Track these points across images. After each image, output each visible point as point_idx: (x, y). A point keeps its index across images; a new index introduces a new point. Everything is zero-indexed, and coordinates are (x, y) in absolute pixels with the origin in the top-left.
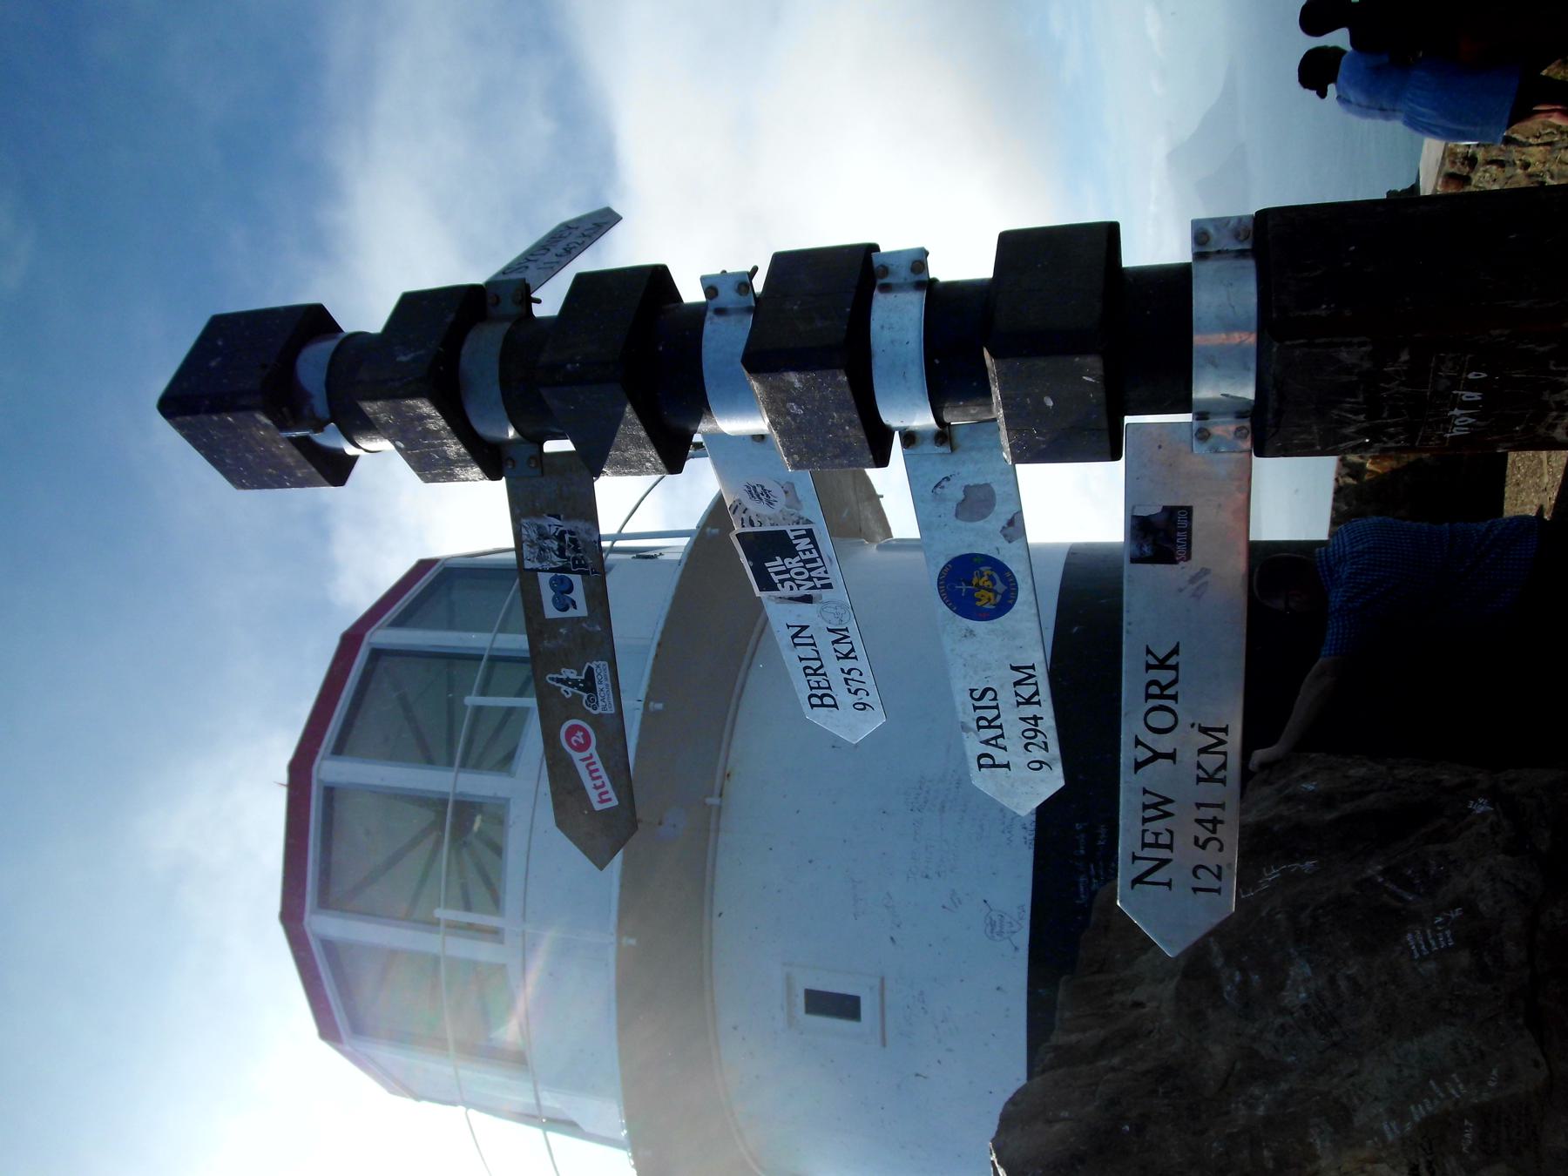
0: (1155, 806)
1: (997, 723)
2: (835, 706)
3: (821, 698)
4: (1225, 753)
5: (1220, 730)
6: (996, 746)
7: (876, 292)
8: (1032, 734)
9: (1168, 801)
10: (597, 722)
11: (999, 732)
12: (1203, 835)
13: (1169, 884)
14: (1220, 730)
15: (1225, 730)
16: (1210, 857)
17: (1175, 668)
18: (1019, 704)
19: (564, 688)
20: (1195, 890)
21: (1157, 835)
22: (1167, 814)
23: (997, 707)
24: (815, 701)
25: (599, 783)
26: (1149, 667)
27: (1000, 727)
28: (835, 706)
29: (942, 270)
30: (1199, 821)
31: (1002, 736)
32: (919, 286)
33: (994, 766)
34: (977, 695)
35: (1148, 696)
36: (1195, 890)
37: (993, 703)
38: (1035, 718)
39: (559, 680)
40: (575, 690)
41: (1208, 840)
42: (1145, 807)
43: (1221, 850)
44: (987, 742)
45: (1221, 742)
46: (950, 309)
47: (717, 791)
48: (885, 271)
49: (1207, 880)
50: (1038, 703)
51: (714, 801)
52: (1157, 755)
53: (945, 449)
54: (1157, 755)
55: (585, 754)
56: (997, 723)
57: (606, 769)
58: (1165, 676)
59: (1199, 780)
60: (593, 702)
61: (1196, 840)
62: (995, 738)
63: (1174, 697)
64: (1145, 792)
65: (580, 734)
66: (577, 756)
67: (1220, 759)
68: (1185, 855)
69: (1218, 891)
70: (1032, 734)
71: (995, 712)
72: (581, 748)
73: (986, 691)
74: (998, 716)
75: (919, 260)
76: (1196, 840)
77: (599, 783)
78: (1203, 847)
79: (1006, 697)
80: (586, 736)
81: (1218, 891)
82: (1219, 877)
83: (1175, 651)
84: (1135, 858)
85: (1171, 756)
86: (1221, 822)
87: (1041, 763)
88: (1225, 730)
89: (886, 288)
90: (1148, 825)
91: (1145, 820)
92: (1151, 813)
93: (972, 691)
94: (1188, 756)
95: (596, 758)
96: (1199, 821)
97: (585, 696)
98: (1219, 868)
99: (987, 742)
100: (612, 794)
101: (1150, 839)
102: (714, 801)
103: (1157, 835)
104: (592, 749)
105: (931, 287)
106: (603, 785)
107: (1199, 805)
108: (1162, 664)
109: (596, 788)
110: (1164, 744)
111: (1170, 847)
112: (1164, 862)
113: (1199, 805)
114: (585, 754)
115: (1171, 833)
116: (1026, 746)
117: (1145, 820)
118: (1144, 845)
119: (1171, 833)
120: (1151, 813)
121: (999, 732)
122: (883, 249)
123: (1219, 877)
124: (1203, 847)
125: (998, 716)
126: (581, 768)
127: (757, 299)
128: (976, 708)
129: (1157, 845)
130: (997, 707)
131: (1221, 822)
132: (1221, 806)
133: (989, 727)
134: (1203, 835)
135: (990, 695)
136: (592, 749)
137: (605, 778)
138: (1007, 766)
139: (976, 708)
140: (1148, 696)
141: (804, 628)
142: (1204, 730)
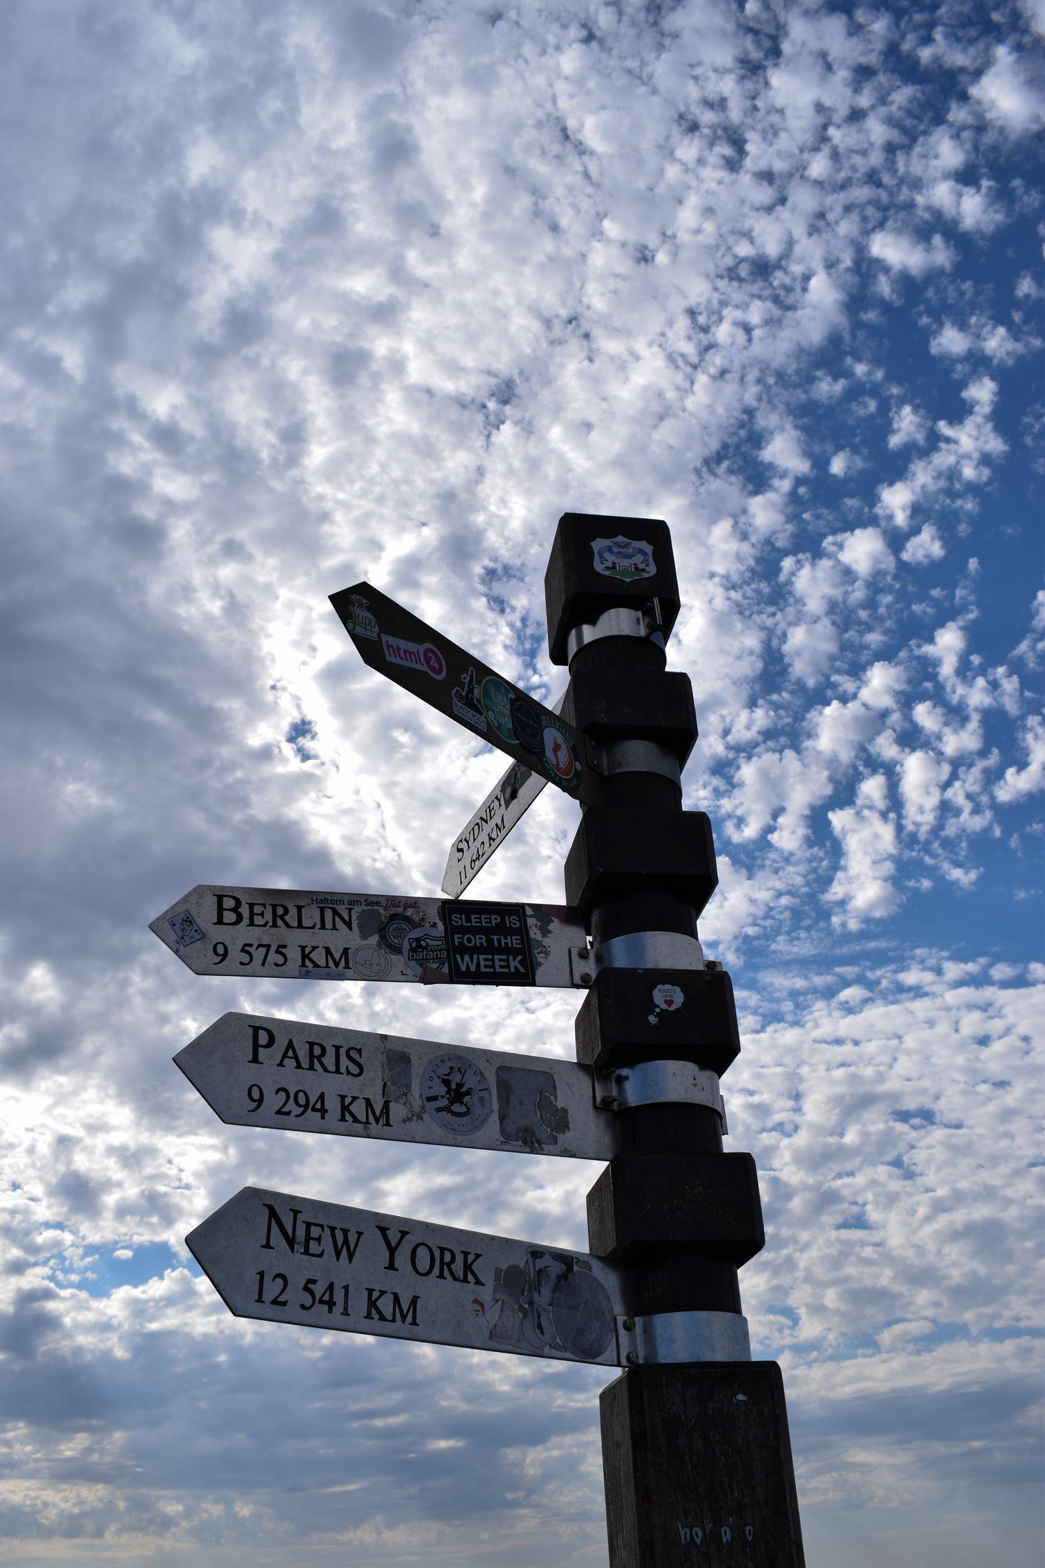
0: (346, 1242)
3: (235, 910)
4: (394, 1321)
5: (414, 1318)
6: (285, 1056)
8: (302, 1100)
9: (351, 1256)
12: (319, 1289)
14: (414, 1318)
15: (414, 1323)
17: (465, 1280)
20: (261, 1274)
22: (338, 1253)
26: (466, 1254)
27: (311, 1068)
30: (331, 1287)
31: (299, 1066)
33: (256, 1046)
34: (354, 1054)
36: (261, 1274)
41: (313, 1295)
42: (345, 1232)
43: (303, 1307)
44: (290, 1045)
45: (404, 1318)
52: (392, 1251)
54: (392, 1251)
58: (458, 1267)
61: (314, 1282)
63: (441, 1276)
64: (360, 1234)
69: (260, 1300)
74: (326, 1070)
76: (314, 1282)
78: (306, 1288)
79: (348, 1086)
81: (260, 1300)
82: (275, 1302)
83: (478, 1282)
85: (391, 1266)
86: (330, 1311)
87: (260, 1101)
90: (327, 1231)
91: (333, 1229)
92: (340, 1238)
93: (359, 1051)
96: (331, 1287)
99: (290, 1045)
101: (315, 1232)
103: (319, 1240)
107: (346, 1288)
108: (468, 1268)
110: (402, 1257)
112: (291, 1242)
113: (346, 1288)
115: (320, 1256)
118: (309, 1225)
119: (320, 1256)
121: (306, 1065)
123: (275, 1302)
124: (306, 1288)
128: (337, 1048)
129: (308, 1238)
131: (330, 1311)
134: (319, 1289)
135: (354, 1069)
138: (255, 1060)
139: (337, 1048)
140: (442, 1250)
142: (414, 1302)
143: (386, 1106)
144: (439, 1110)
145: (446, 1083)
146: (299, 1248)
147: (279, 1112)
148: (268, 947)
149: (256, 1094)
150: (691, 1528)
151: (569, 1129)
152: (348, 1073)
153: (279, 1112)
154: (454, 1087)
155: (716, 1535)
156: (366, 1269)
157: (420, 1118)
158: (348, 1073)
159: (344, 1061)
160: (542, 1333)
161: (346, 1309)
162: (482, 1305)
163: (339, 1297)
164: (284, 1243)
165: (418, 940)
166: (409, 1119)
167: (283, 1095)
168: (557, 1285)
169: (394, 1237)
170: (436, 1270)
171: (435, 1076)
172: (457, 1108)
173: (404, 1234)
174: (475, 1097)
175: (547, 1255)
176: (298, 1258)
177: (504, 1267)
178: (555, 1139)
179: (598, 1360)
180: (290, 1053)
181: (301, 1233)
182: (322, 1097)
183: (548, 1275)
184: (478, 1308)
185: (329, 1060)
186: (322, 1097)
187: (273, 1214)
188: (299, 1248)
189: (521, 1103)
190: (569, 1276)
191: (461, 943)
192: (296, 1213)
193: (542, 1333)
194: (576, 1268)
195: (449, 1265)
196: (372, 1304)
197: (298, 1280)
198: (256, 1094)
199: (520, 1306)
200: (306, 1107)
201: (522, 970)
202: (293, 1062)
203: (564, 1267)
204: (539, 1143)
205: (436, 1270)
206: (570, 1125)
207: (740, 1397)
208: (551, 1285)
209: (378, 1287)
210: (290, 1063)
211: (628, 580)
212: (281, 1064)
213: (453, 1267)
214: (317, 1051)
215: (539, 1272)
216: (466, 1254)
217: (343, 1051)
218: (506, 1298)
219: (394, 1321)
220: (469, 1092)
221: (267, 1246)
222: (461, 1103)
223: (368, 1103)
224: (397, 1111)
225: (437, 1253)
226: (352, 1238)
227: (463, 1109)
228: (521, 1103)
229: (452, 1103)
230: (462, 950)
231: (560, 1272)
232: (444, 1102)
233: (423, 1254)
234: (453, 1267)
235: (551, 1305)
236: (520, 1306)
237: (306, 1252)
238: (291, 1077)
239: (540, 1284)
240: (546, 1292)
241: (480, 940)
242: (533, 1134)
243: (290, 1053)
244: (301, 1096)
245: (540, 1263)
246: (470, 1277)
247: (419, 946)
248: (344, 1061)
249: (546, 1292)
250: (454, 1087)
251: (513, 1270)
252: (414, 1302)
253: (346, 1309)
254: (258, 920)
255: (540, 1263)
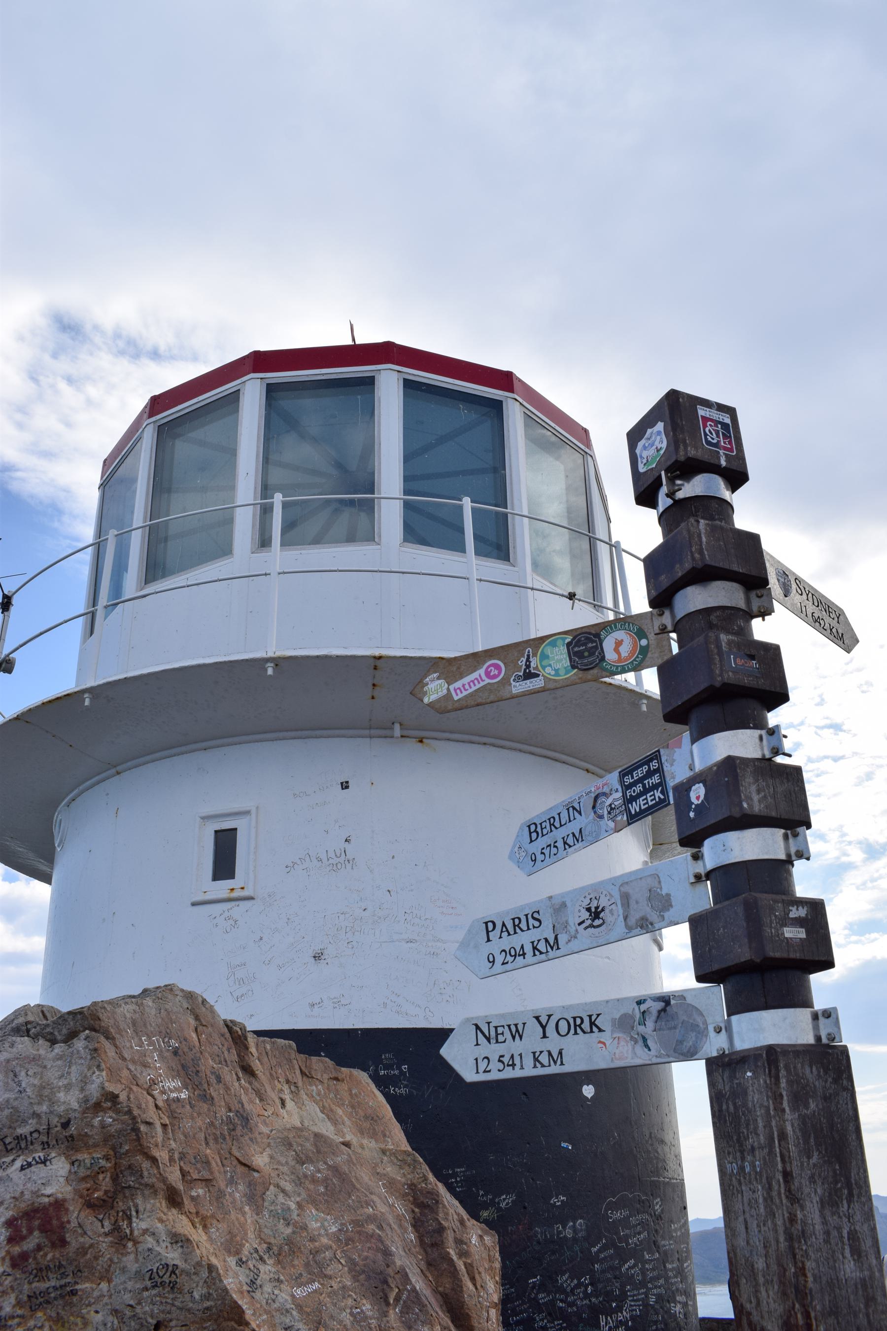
0: (517, 1031)
1: (518, 930)
2: (531, 841)
3: (536, 831)
4: (550, 1066)
5: (562, 1062)
6: (502, 931)
7: (783, 831)
8: (513, 953)
9: (521, 1037)
10: (505, 682)
11: (512, 932)
12: (506, 1060)
13: (477, 1044)
14: (562, 1062)
15: (562, 1064)
16: (495, 1065)
17: (592, 1031)
18: (533, 943)
19: (525, 660)
20: (476, 1059)
21: (502, 1034)
22: (514, 1038)
23: (529, 929)
24: (533, 828)
25: (467, 687)
26: (590, 1016)
27: (515, 933)
28: (531, 841)
29: (799, 868)
30: (512, 1057)
31: (509, 934)
32: (789, 855)
33: (488, 932)
34: (536, 915)
35: (575, 1018)
36: (476, 1059)
37: (531, 927)
38: (524, 954)
39: (528, 656)
40: (524, 667)
41: (503, 1063)
42: (516, 1025)
43: (499, 1071)
44: (504, 925)
45: (555, 1062)
46: (775, 873)
47: (405, 733)
48: (796, 835)
49: (482, 1065)
50: (535, 955)
51: (397, 731)
52: (544, 1027)
53: (693, 880)
54: (544, 1027)
55: (484, 677)
56: (518, 930)
57: (476, 691)
58: (586, 1026)
59: (534, 1053)
60: (518, 679)
61: (502, 1056)
62: (507, 931)
63: (576, 1033)
64: (524, 1024)
65: (496, 672)
66: (482, 671)
67: (546, 1063)
68: (493, 1050)
69: (477, 1072)
70: (513, 953)
71: (525, 928)
72: (487, 674)
73: (540, 921)
74: (522, 931)
75: (803, 854)
76: (502, 1056)
77: (467, 687)
78: (499, 1061)
79: (534, 935)
80: (495, 677)
81: (477, 1072)
82: (485, 1071)
83: (600, 1030)
84: (489, 1023)
85: (545, 1036)
86: (513, 1069)
87: (494, 961)
88: (562, 1064)
89: (786, 837)
90: (506, 1028)
91: (509, 1026)
92: (513, 1029)
93: (538, 912)
94: (546, 1045)
95: (482, 684)
96: (512, 1057)
97: (521, 674)
98: (489, 1071)
99: (504, 925)
100: (460, 696)
101: (500, 1030)
102: (397, 731)
103: (502, 1034)
104: (488, 681)
105: (789, 862)
106: (466, 690)
107: (521, 1055)
108: (592, 1024)
109: (464, 686)
111: (497, 1042)
112: (488, 1039)
113: (521, 1055)
114: (484, 677)
115: (504, 1042)
116: (504, 951)
117: (509, 1026)
118: (496, 1028)
119: (504, 1042)
120: (513, 1029)
121: (512, 932)
122: (808, 832)
123: (485, 1071)
124: (499, 1061)
125: (522, 931)
126: (475, 675)
127: (770, 759)
128: (526, 915)
129: (497, 1034)
130: (529, 929)
131: (513, 1069)
132: (522, 1068)
133: (514, 926)
135: (537, 924)
136: (488, 681)
137: (470, 691)
138: (489, 940)
139: (526, 915)
140: (575, 1018)
141: (580, 813)
142: (560, 1053)
143: (556, 938)
144: (586, 928)
145: (589, 910)
146: (493, 1041)
147: (503, 964)
148: (550, 845)
149: (491, 959)
150: (732, 1163)
151: (671, 906)
152: (534, 927)
153: (503, 964)
154: (593, 910)
155: (742, 1168)
156: (784, 1151)
157: (576, 937)
158: (534, 927)
159: (531, 921)
160: (650, 1050)
161: (522, 1066)
162: (604, 1044)
163: (517, 1060)
164: (485, 1040)
165: (610, 805)
166: (569, 941)
167: (503, 953)
168: (658, 1017)
169: (544, 1020)
170: (572, 1031)
171: (581, 908)
172: (597, 922)
173: (549, 1016)
174: (607, 911)
175: (649, 1000)
176: (494, 1046)
177: (617, 1017)
178: (663, 917)
179: (695, 1057)
180: (504, 929)
181: (493, 1033)
182: (522, 947)
183: (650, 1013)
184: (602, 1045)
185: (523, 925)
186: (522, 947)
187: (477, 1027)
188: (493, 1041)
189: (637, 902)
190: (668, 1008)
191: (631, 795)
192: (489, 1023)
193: (650, 1050)
194: (673, 1002)
195: (580, 1026)
196: (536, 1059)
197: (494, 1058)
198: (491, 959)
199: (632, 1037)
200: (515, 956)
201: (662, 797)
202: (506, 933)
203: (663, 1004)
204: (652, 924)
205: (572, 1031)
206: (673, 904)
207: (749, 1074)
208: (654, 1018)
209: (538, 1050)
210: (505, 934)
211: (654, 466)
212: (501, 937)
213: (583, 1026)
214: (517, 921)
215: (644, 1012)
216: (590, 1016)
217: (529, 916)
218: (620, 1035)
219: (550, 1066)
220: (603, 910)
221: (477, 1044)
222: (599, 918)
223: (546, 940)
224: (562, 939)
225: (571, 1021)
226: (520, 1028)
227: (601, 921)
228: (637, 902)
229: (593, 921)
230: (633, 799)
231: (660, 1008)
232: (589, 922)
233: (563, 1026)
234: (583, 1026)
235: (655, 1030)
236: (632, 1037)
237: (497, 1042)
238: (507, 942)
239: (644, 1020)
240: (650, 1024)
241: (639, 788)
242: (647, 920)
243: (504, 929)
244: (512, 951)
245: (643, 1007)
246: (595, 1029)
247: (612, 809)
248: (531, 921)
249: (650, 1024)
250: (593, 910)
251: (625, 1017)
252: (560, 1053)
253: (522, 1066)
254: (501, 1038)
255: (643, 1007)
